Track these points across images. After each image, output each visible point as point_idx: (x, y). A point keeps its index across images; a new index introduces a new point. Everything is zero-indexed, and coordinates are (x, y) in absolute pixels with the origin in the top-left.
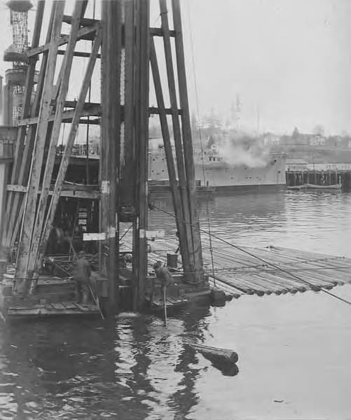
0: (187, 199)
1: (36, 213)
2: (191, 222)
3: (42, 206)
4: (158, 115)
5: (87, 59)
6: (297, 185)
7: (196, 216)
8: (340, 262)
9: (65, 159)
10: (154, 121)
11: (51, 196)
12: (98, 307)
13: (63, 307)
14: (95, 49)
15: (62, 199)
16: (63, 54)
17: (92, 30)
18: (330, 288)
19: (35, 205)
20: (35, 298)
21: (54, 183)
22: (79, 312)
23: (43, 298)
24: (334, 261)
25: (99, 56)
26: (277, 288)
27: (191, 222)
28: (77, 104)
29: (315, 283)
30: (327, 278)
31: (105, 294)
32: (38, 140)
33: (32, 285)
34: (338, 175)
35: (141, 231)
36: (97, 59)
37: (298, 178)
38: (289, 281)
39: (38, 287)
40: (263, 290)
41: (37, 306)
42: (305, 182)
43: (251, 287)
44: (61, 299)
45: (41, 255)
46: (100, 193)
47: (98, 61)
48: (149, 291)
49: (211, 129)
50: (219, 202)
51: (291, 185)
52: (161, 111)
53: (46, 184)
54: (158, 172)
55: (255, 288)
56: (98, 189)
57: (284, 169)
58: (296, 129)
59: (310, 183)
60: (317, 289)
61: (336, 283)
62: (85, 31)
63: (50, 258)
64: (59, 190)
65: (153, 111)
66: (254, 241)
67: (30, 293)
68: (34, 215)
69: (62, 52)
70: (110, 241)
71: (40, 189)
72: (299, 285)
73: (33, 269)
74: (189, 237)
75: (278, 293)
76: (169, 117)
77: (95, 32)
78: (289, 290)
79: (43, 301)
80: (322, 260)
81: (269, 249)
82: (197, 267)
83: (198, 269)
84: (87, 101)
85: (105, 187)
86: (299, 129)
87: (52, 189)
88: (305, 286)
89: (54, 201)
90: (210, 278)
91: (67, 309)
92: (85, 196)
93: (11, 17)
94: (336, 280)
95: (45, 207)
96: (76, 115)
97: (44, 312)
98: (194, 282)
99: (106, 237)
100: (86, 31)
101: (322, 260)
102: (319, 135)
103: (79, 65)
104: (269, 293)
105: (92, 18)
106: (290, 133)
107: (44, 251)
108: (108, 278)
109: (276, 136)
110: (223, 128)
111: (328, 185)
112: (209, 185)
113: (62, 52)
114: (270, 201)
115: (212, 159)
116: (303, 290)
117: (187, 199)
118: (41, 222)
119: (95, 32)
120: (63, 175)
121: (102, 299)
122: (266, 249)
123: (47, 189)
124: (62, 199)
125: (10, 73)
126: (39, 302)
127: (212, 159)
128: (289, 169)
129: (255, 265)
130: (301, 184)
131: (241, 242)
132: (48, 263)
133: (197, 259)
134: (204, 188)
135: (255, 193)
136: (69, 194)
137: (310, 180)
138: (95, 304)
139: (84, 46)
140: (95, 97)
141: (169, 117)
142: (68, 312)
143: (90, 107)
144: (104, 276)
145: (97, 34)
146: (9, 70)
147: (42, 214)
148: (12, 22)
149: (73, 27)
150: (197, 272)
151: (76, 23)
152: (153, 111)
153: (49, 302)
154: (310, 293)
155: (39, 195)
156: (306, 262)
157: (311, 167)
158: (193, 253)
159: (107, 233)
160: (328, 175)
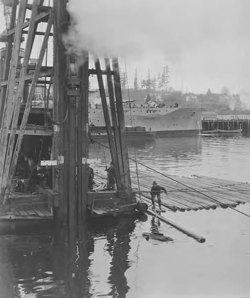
0: (122, 138)
1: (7, 146)
2: (122, 152)
3: (11, 141)
4: (96, 75)
5: (43, 37)
6: (210, 130)
7: (125, 148)
8: (244, 187)
9: (28, 107)
10: (93, 80)
11: (18, 135)
12: (52, 214)
13: (26, 214)
14: (49, 29)
15: (25, 136)
16: (44, 35)
17: (47, 14)
18: (234, 206)
19: (6, 141)
20: (7, 207)
21: (20, 125)
22: (38, 218)
23: (13, 208)
24: (239, 185)
25: (51, 35)
26: (197, 206)
27: (122, 152)
28: (36, 67)
29: (224, 202)
30: (232, 199)
31: (57, 205)
32: (8, 94)
33: (5, 197)
34: (240, 123)
35: (83, 159)
36: (50, 37)
37: (211, 124)
38: (203, 201)
39: (9, 200)
40: (177, 205)
41: (8, 213)
42: (215, 128)
43: (175, 205)
44: (25, 209)
45: (11, 176)
46: (54, 131)
47: (51, 39)
48: (89, 202)
49: (148, 90)
50: (159, 142)
51: (205, 130)
52: (98, 72)
53: (15, 125)
54: (95, 117)
55: (192, 206)
56: (52, 129)
57: (200, 118)
58: (209, 90)
59: (220, 129)
60: (224, 206)
61: (239, 203)
62: (42, 15)
63: (22, 180)
64: (23, 129)
65: (92, 72)
66: (180, 171)
67: (4, 204)
68: (6, 147)
69: (26, 32)
70: (60, 167)
71: (10, 129)
72: (212, 204)
73: (5, 186)
74: (120, 164)
75: (196, 210)
76: (104, 77)
77: (49, 15)
78: (204, 208)
79: (13, 210)
80: (231, 185)
81: (193, 177)
82: (127, 185)
83: (128, 187)
84: (43, 64)
85: (56, 129)
86: (211, 90)
87: (18, 129)
88: (216, 204)
89: (20, 138)
90: (137, 194)
91: (31, 215)
92: (44, 134)
93: (5, 10)
94: (240, 200)
95: (13, 142)
96: (35, 76)
97: (13, 217)
98: (124, 196)
99: (58, 163)
100: (43, 15)
101: (231, 185)
102: (225, 94)
103: (39, 40)
104: (189, 210)
105: (48, 6)
106: (205, 92)
107: (13, 173)
108: (59, 192)
109: (195, 95)
110: (157, 89)
111: (232, 130)
112: (152, 130)
113: (26, 32)
114: (191, 141)
115: (149, 112)
116: (214, 208)
117: (122, 138)
118: (11, 153)
119: (49, 15)
120: (26, 119)
121: (54, 207)
122: (191, 177)
123: (14, 129)
124: (25, 136)
125: (3, 50)
126: (10, 211)
127: (149, 112)
128: (204, 119)
129: (181, 189)
130: (212, 130)
131: (171, 172)
132: (20, 184)
133: (127, 180)
134: (148, 132)
135: (180, 137)
136: (31, 133)
137: (219, 126)
138: (50, 212)
139: (42, 27)
140: (50, 64)
141: (104, 77)
142: (30, 218)
143: (45, 69)
144: (56, 191)
145: (50, 16)
146: (3, 48)
147: (11, 147)
148: (5, 14)
149: (33, 11)
150: (126, 190)
151: (35, 9)
152: (92, 72)
153: (18, 210)
154: (219, 209)
155: (9, 134)
156: (219, 187)
157: (220, 117)
158: (124, 176)
159: (58, 161)
160: (232, 123)
